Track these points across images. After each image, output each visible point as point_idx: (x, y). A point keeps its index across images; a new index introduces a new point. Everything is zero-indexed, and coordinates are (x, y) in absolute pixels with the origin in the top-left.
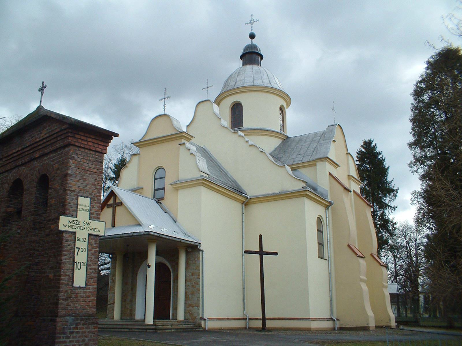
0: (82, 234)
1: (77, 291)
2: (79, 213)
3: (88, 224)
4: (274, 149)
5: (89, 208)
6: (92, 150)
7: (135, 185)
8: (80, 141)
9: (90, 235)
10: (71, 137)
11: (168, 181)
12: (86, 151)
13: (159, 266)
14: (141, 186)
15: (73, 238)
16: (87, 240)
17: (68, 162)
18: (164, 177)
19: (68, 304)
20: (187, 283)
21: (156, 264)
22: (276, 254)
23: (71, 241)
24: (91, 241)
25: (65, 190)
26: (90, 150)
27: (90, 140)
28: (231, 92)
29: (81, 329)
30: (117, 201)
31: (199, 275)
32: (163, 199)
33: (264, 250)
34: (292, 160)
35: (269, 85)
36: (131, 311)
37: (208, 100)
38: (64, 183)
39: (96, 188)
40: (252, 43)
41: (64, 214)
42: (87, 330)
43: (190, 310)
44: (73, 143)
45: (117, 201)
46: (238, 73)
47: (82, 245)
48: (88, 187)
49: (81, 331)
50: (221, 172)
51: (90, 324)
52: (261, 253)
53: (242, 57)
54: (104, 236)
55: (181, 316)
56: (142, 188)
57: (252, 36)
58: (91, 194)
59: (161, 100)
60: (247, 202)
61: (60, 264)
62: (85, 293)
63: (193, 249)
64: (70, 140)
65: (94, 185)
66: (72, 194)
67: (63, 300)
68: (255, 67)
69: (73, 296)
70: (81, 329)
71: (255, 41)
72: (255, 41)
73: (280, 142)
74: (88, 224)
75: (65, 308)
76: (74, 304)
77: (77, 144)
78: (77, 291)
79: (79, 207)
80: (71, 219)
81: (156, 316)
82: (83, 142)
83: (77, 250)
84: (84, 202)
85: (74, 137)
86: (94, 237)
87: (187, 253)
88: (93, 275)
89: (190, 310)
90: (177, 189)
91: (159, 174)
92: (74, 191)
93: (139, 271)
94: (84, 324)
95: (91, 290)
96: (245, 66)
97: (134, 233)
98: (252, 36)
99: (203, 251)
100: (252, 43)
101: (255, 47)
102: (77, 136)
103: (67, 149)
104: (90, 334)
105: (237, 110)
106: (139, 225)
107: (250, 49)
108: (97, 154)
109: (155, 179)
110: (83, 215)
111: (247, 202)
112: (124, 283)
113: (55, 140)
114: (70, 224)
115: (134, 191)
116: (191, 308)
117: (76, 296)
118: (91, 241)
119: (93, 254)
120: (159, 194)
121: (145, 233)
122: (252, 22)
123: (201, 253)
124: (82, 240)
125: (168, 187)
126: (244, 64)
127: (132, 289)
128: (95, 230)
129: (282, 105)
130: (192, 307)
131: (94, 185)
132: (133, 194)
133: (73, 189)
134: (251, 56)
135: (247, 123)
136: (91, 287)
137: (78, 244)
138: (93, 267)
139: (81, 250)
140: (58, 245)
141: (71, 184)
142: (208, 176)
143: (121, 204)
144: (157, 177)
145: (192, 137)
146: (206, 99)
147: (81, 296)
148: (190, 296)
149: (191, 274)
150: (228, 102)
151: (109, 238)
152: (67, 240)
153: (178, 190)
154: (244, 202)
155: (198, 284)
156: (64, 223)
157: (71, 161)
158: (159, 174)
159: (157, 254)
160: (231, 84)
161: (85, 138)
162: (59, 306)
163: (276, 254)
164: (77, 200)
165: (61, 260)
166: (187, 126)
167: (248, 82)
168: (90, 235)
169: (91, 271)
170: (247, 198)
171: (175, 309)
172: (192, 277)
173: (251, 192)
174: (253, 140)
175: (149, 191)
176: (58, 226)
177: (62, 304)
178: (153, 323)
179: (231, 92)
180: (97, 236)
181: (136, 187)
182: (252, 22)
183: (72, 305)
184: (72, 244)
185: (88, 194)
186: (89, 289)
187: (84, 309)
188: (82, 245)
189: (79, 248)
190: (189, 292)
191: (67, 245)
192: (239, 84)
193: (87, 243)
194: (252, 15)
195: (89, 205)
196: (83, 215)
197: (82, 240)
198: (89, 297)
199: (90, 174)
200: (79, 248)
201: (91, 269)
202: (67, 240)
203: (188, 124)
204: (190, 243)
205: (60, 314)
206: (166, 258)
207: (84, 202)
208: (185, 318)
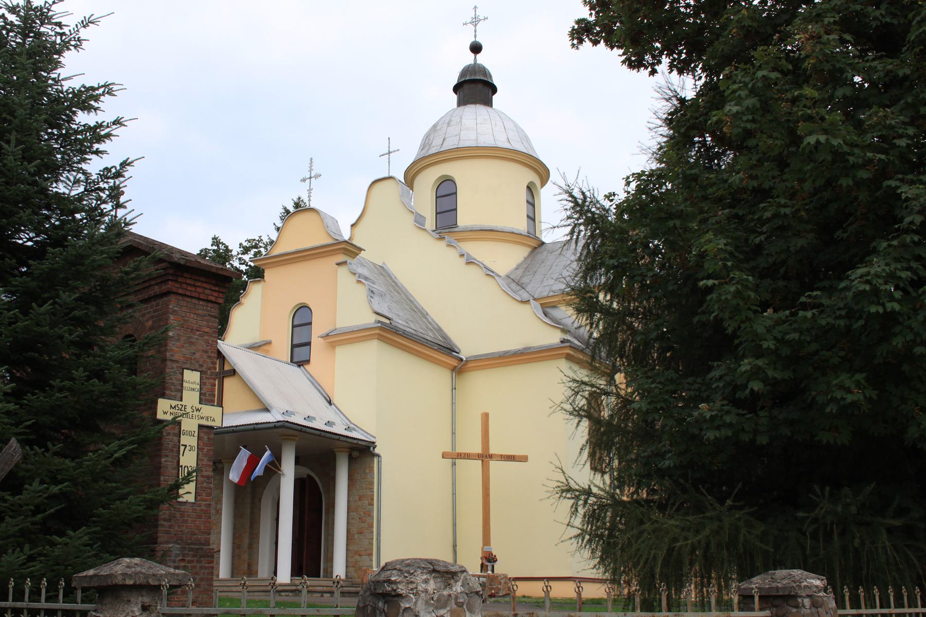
0: (190, 425)
1: (183, 508)
2: (185, 394)
3: (198, 410)
4: (515, 266)
5: (198, 387)
6: (203, 300)
7: (256, 338)
8: (185, 286)
9: (200, 426)
10: (172, 280)
11: (319, 328)
12: (194, 300)
13: (301, 485)
14: (267, 339)
15: (176, 431)
16: (196, 434)
17: (167, 319)
18: (310, 324)
19: (170, 526)
20: (353, 514)
21: (296, 480)
22: (524, 459)
23: (174, 435)
24: (202, 435)
25: (164, 360)
26: (199, 299)
27: (199, 284)
28: (435, 159)
29: (189, 562)
30: (226, 368)
31: (373, 499)
32: (308, 362)
33: (492, 451)
34: (548, 288)
35: (507, 146)
36: (249, 565)
37: (390, 178)
38: (163, 349)
39: (209, 357)
40: (475, 63)
41: (163, 396)
42: (198, 565)
43: (357, 562)
44: (175, 290)
45: (226, 368)
46: (448, 120)
47: (189, 441)
48: (197, 356)
49: (189, 565)
50: (413, 313)
51: (201, 557)
52: (485, 457)
53: (456, 89)
54: (221, 428)
55: (339, 569)
56: (269, 343)
57: (476, 48)
58: (201, 366)
59: (304, 180)
60: (460, 367)
61: (160, 468)
62: (194, 511)
63: (361, 453)
64: (170, 286)
65: (206, 352)
66: (175, 365)
67: (165, 520)
68: (481, 109)
69: (178, 515)
70: (189, 562)
71: (481, 59)
72: (481, 59)
73: (521, 259)
74: (198, 410)
75: (168, 532)
76: (179, 526)
77: (180, 291)
78: (183, 508)
79: (185, 384)
80: (174, 403)
81: (297, 570)
82: (189, 288)
83: (182, 448)
84: (192, 378)
85: (176, 281)
86: (205, 430)
87: (351, 460)
88: (205, 485)
89: (357, 562)
90: (333, 345)
91: (302, 318)
92: (177, 362)
93: (266, 491)
94: (194, 556)
95: (203, 508)
96: (462, 108)
97: (257, 424)
98: (476, 48)
99: (378, 456)
100: (475, 63)
101: (484, 71)
102: (180, 280)
103: (165, 299)
104: (203, 571)
105: (446, 193)
106: (267, 410)
107: (471, 75)
108: (210, 305)
109: (293, 326)
110: (191, 398)
111: (460, 367)
112: (237, 515)
113: (147, 285)
114: (172, 411)
115: (254, 347)
116: (357, 557)
117: (182, 516)
118: (202, 435)
119: (206, 455)
120: (301, 353)
121: (256, 427)
122: (475, 21)
123: (376, 460)
124: (190, 434)
125: (316, 341)
126: (461, 103)
127: (252, 527)
128: (207, 419)
129: (532, 183)
130: (360, 555)
131: (206, 352)
132: (252, 354)
133: (176, 357)
134: (475, 87)
135: (464, 219)
136: (203, 503)
137: (184, 440)
138: (205, 474)
139: (188, 448)
140: (157, 439)
141: (172, 350)
142: (388, 322)
143: (233, 372)
144: (296, 323)
145: (361, 249)
146: (386, 175)
147: (188, 516)
148: (356, 536)
149: (357, 498)
150: (428, 180)
151: (275, 427)
152: (169, 434)
153: (334, 347)
154: (455, 367)
155: (369, 514)
156: (164, 408)
157: (172, 317)
158: (302, 318)
159: (298, 462)
160: (434, 144)
161: (192, 282)
162: (159, 529)
163: (524, 459)
164: (182, 374)
165: (160, 463)
166: (352, 226)
167: (468, 139)
168: (200, 426)
169: (203, 479)
170: (462, 360)
171: (330, 560)
172: (359, 503)
173: (469, 346)
174: (477, 249)
175: (282, 346)
176: (156, 413)
177: (162, 525)
178: (289, 582)
179: (435, 159)
180: (211, 428)
181: (258, 341)
182: (475, 21)
183: (176, 528)
184: (176, 439)
185: (197, 366)
186: (200, 505)
187: (193, 534)
188: (189, 441)
189: (186, 446)
190: (354, 530)
191: (168, 441)
192: (449, 144)
193: (196, 438)
194: (475, 7)
195: (198, 381)
196: (191, 398)
197: (190, 434)
198: (199, 517)
199: (200, 335)
200: (186, 446)
201: (202, 476)
202: (169, 434)
203: (353, 221)
204: (356, 442)
205: (159, 540)
206: (312, 470)
207: (192, 378)
208: (346, 576)
